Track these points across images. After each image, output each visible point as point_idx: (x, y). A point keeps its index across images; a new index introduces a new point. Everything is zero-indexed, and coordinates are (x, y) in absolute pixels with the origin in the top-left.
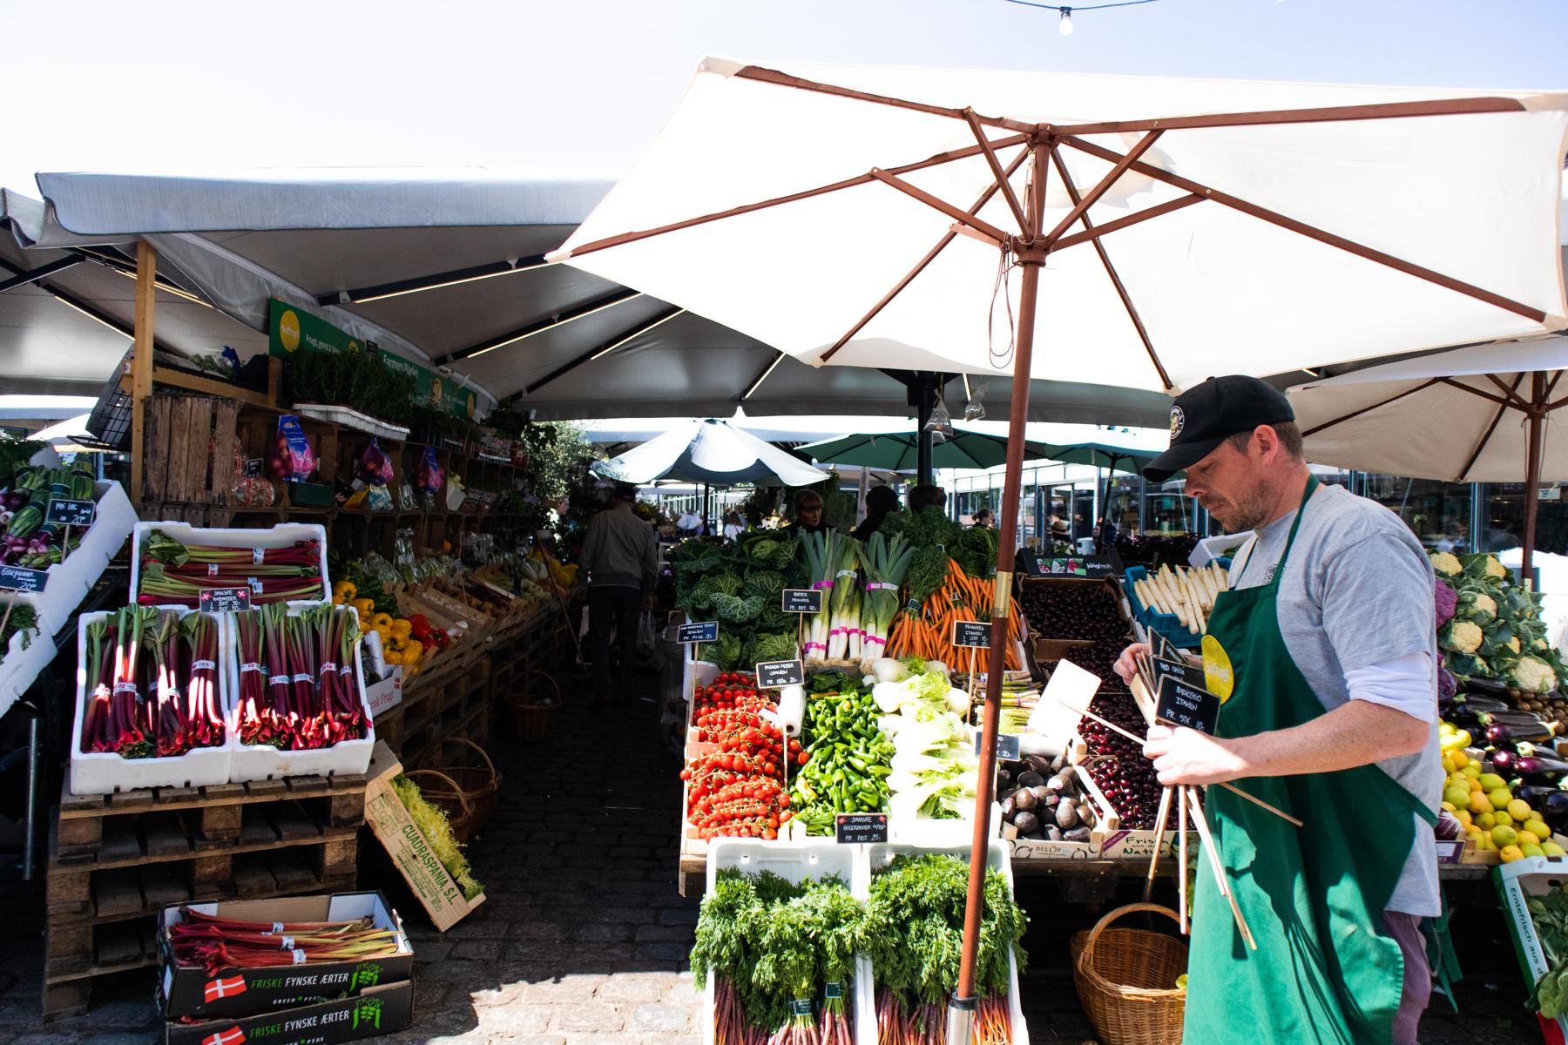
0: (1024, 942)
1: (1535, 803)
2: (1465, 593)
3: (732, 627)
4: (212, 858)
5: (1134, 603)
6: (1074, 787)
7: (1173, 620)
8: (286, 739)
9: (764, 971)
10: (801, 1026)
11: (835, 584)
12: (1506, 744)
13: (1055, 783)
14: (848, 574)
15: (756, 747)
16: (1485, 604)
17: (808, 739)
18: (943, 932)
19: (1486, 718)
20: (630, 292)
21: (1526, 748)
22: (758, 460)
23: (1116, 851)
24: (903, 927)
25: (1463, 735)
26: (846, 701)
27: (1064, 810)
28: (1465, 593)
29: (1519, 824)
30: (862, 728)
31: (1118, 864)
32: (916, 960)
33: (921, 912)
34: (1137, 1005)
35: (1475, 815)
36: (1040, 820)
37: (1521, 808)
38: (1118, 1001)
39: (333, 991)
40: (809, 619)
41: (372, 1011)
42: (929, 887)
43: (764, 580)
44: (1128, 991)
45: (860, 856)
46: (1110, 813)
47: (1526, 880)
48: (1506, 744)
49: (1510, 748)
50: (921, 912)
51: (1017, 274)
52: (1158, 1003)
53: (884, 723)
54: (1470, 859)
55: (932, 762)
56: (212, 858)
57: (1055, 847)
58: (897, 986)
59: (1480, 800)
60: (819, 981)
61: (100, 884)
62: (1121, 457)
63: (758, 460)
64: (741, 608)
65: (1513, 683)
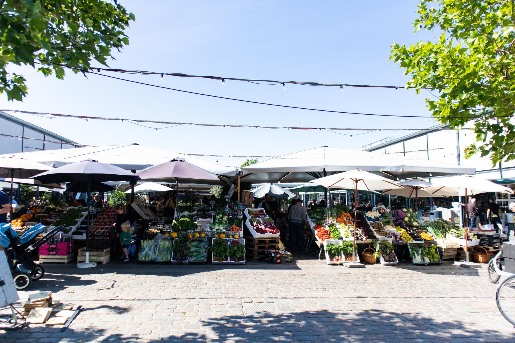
0: (358, 249)
1: (412, 237)
2: (407, 214)
3: (318, 219)
4: (267, 246)
5: (365, 216)
6: (361, 236)
7: (370, 217)
8: (273, 232)
9: (333, 252)
10: (337, 257)
11: (328, 214)
12: (409, 231)
13: (359, 235)
14: (330, 213)
15: (325, 232)
16: (409, 215)
17: (330, 231)
18: (350, 248)
19: (408, 228)
20: (289, 173)
21: (412, 231)
22: (441, 212)
23: (366, 242)
24: (346, 247)
25: (405, 230)
26: (334, 227)
27: (360, 238)
28: (407, 214)
29: (410, 239)
30: (335, 230)
31: (366, 243)
32: (347, 251)
33: (347, 246)
34: (369, 256)
35: (405, 238)
36: (358, 239)
37: (410, 237)
38: (367, 256)
39: (286, 257)
40: (326, 219)
41: (289, 260)
42: (348, 244)
43: (320, 214)
44: (368, 255)
45: (340, 241)
46: (365, 238)
47: (410, 244)
48: (409, 231)
49: (410, 231)
50: (347, 246)
51: (355, 183)
52: (371, 256)
53: (338, 230)
54: (404, 243)
55: (345, 233)
56: (267, 246)
57: (360, 241)
58: (346, 253)
59: (406, 236)
60: (338, 253)
61: (259, 248)
62: (500, 288)
63: (441, 212)
64: (318, 217)
65: (413, 225)
